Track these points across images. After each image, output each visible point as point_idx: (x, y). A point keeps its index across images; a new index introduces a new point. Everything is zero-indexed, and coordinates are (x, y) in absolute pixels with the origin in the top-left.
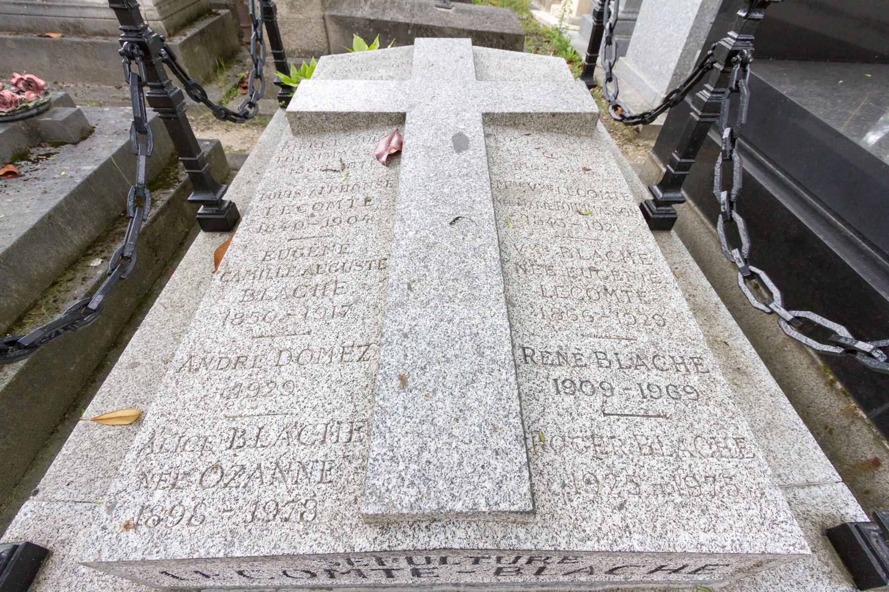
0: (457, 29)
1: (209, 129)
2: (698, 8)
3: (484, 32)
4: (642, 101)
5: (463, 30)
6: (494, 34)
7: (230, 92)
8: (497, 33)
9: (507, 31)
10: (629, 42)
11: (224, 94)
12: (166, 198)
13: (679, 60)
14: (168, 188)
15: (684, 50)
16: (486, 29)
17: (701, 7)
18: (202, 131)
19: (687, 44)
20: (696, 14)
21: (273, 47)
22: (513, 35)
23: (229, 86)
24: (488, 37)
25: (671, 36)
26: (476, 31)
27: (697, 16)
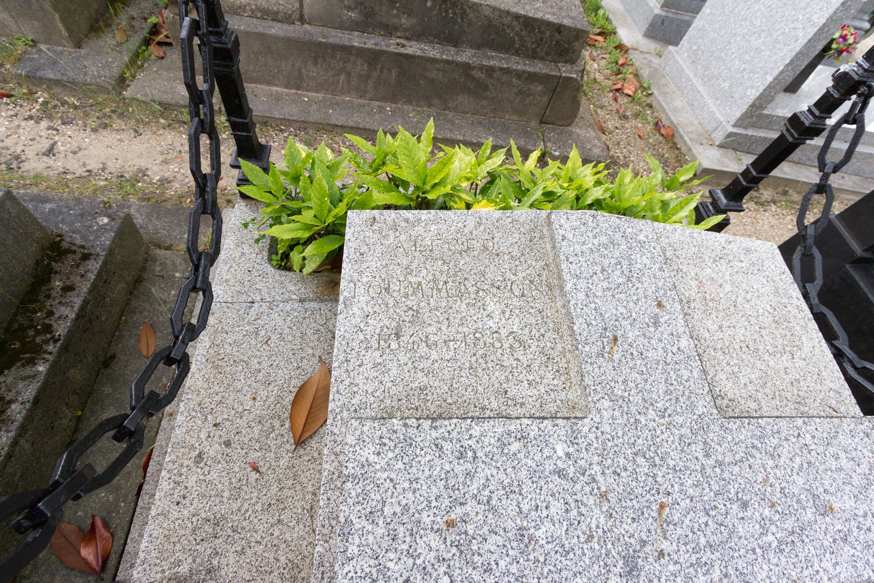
0: (500, 10)
1: (105, 126)
2: (815, 30)
3: (535, 20)
4: (696, 122)
5: (508, 12)
6: (549, 24)
7: (137, 55)
8: (554, 24)
9: (566, 22)
10: (688, 24)
11: (126, 59)
12: (29, 392)
13: (765, 90)
14: (32, 362)
15: (775, 79)
16: (539, 15)
17: (819, 29)
18: (94, 130)
19: (782, 72)
20: (810, 37)
21: (230, 113)
22: (575, 29)
23: (135, 42)
24: (539, 28)
25: (758, 50)
26: (525, 16)
27: (810, 40)
